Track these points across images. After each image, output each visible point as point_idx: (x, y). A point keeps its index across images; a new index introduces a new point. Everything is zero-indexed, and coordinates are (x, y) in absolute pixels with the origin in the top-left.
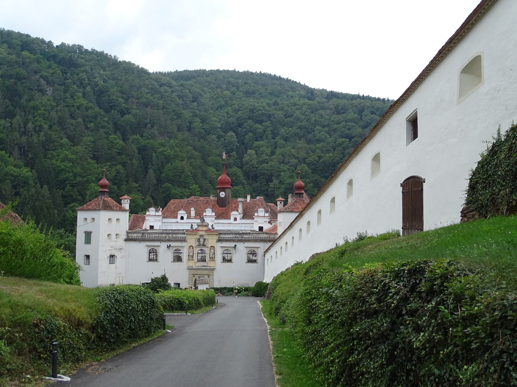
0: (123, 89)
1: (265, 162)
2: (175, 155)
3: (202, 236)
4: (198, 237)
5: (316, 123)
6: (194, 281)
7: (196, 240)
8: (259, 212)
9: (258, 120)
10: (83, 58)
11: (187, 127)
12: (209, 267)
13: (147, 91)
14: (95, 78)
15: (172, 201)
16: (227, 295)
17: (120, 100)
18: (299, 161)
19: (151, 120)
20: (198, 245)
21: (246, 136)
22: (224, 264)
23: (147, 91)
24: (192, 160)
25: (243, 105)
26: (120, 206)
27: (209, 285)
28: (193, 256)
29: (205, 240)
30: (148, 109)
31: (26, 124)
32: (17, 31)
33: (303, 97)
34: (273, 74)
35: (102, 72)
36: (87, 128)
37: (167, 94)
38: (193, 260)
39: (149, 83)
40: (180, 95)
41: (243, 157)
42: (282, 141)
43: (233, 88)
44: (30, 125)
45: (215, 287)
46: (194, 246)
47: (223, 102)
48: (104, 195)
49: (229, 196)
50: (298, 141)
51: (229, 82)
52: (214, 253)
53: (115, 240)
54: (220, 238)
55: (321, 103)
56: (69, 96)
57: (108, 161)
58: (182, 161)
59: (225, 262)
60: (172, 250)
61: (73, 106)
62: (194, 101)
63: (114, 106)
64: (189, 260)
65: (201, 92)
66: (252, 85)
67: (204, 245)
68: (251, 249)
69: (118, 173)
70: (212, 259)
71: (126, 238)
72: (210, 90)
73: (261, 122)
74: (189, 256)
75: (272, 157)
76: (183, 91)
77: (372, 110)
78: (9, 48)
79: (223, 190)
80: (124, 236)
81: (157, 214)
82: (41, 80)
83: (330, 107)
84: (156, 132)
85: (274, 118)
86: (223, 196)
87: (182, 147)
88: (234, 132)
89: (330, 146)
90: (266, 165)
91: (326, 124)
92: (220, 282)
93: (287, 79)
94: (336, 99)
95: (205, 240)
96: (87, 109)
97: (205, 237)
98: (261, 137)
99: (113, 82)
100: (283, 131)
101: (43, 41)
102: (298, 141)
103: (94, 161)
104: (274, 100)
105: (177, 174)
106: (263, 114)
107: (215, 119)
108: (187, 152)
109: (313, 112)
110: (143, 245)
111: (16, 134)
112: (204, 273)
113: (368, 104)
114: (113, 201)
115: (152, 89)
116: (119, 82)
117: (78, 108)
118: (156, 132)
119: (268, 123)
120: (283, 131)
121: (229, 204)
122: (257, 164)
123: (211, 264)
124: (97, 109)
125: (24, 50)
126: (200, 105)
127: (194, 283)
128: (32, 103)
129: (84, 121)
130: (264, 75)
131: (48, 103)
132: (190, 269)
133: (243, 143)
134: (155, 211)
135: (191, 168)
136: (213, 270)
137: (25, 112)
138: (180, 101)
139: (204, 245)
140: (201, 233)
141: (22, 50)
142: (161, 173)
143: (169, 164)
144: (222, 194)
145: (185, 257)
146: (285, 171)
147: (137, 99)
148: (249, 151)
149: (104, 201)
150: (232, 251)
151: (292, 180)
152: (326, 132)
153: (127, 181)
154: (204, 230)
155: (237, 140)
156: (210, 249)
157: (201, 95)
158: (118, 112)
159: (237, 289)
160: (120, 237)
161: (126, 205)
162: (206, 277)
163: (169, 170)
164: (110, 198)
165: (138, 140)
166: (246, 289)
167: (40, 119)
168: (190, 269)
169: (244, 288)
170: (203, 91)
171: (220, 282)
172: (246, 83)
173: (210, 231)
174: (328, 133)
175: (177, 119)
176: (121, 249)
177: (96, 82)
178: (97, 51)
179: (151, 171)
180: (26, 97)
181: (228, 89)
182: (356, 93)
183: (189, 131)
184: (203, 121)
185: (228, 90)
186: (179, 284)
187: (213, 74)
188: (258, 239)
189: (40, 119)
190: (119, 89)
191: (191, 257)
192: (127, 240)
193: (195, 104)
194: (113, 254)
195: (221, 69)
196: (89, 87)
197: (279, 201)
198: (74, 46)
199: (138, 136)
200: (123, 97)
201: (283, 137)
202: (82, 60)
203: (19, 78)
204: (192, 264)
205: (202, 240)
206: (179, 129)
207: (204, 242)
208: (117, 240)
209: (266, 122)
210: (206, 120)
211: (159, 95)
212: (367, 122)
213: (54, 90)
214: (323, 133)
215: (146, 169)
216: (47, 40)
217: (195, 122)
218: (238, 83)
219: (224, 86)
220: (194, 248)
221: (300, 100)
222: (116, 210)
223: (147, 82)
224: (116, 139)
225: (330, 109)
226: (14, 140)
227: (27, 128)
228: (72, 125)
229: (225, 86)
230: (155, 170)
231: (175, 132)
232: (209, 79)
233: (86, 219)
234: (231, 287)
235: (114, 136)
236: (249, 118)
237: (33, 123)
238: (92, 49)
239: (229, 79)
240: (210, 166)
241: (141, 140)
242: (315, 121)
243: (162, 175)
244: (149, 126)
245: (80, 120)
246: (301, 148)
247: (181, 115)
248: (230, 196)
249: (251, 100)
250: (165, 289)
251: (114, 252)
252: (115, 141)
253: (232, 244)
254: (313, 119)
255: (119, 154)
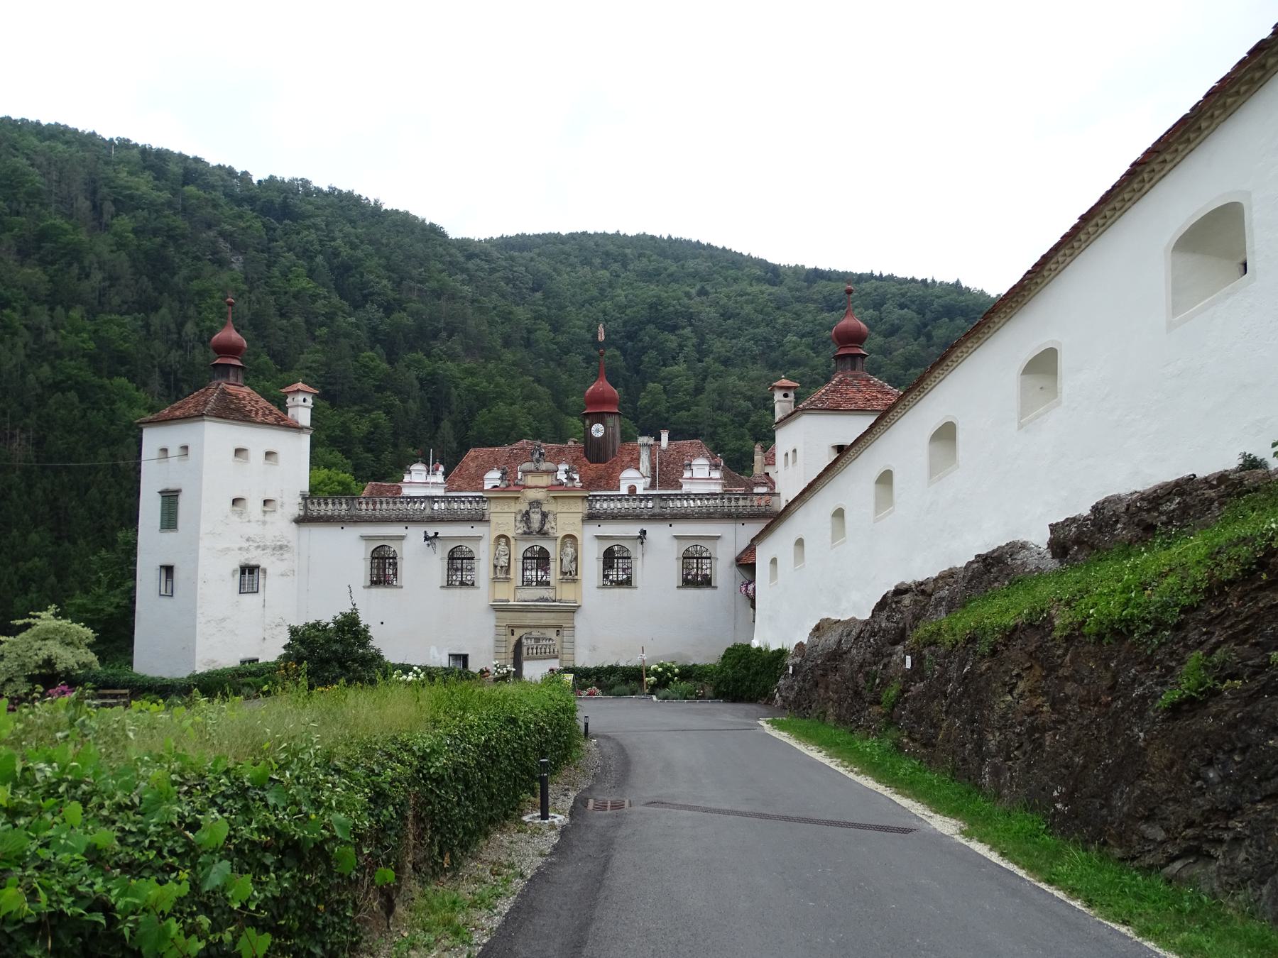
0: (391, 263)
1: (684, 409)
2: (497, 392)
3: (535, 503)
4: (525, 507)
5: (786, 330)
6: (511, 648)
7: (519, 517)
8: (693, 467)
9: (668, 325)
10: (310, 203)
11: (522, 338)
12: (560, 601)
13: (440, 266)
14: (334, 239)
15: (472, 452)
16: (619, 695)
17: (385, 282)
18: (755, 406)
19: (447, 324)
20: (525, 533)
21: (643, 358)
22: (607, 591)
23: (440, 266)
24: (532, 402)
25: (636, 296)
26: (280, 413)
27: (562, 660)
28: (507, 569)
29: (545, 516)
30: (442, 302)
31: (180, 326)
32: (176, 151)
33: (759, 280)
34: (694, 240)
35: (348, 229)
36: (314, 338)
37: (481, 274)
38: (508, 580)
39: (444, 253)
40: (508, 278)
41: (638, 399)
42: (717, 364)
43: (616, 264)
44: (190, 328)
45: (579, 664)
46: (510, 535)
47: (595, 292)
48: (228, 376)
49: (614, 435)
50: (750, 366)
51: (607, 254)
52: (576, 559)
53: (260, 517)
54: (594, 511)
55: (797, 290)
56: (277, 274)
57: (355, 404)
58: (512, 404)
59: (611, 587)
60: (442, 551)
61: (286, 293)
62: (534, 290)
63: (372, 294)
64: (495, 579)
65: (550, 271)
66: (654, 257)
67: (542, 533)
68: (695, 542)
69: (376, 426)
70: (570, 576)
71: (302, 513)
72: (569, 269)
73: (674, 329)
74: (495, 566)
75: (698, 398)
76: (515, 269)
77: (902, 300)
78: (156, 179)
79: (600, 418)
80: (294, 507)
81: (432, 479)
82: (221, 240)
83: (815, 297)
84: (458, 348)
85: (700, 320)
86: (600, 435)
87: (513, 377)
88: (618, 348)
89: (818, 374)
90: (686, 413)
91: (808, 329)
92: (594, 649)
93: (724, 248)
94: (824, 282)
95: (545, 516)
96: (315, 298)
97: (545, 508)
98: (674, 358)
99: (371, 249)
100: (718, 346)
101: (230, 172)
102: (750, 366)
103: (327, 404)
104: (698, 287)
105: (501, 430)
106: (676, 313)
107: (578, 323)
108: (522, 386)
109: (778, 308)
110: (351, 535)
111: (158, 346)
112: (543, 623)
113: (893, 290)
114: (256, 396)
115: (451, 263)
116: (383, 249)
117: (296, 297)
118: (458, 348)
119: (687, 331)
120: (718, 346)
121: (614, 455)
122: (668, 412)
123: (566, 593)
124: (335, 299)
125: (188, 184)
126: (549, 298)
127: (512, 655)
128: (196, 285)
129: (307, 321)
130: (679, 242)
131: (233, 284)
132: (499, 608)
133: (638, 372)
134: (425, 473)
135: (530, 418)
136: (573, 610)
137: (181, 302)
138: (509, 289)
139: (542, 533)
140: (532, 495)
141: (185, 183)
142: (468, 428)
143: (484, 410)
144: (598, 430)
145: (483, 569)
146: (725, 425)
147: (420, 282)
148: (650, 385)
149: (223, 392)
150: (635, 549)
151: (741, 442)
152: (808, 346)
153: (395, 446)
154: (543, 484)
155: (624, 364)
156: (563, 545)
157: (551, 278)
158: (380, 306)
159: (655, 673)
160: (279, 510)
161: (302, 411)
162: (551, 633)
163: (484, 423)
164: (247, 389)
165: (419, 361)
166: (688, 673)
167: (211, 316)
168: (499, 608)
169: (679, 668)
170: (555, 270)
171: (594, 649)
172: (640, 255)
173: (562, 488)
174: (812, 349)
175: (502, 323)
176: (281, 547)
177: (336, 249)
178: (340, 191)
179: (446, 425)
180: (184, 272)
181: (604, 266)
182: (867, 271)
183: (526, 347)
184: (556, 328)
185: (606, 269)
186: (465, 658)
187: (574, 239)
188: (716, 512)
189: (211, 316)
190: (383, 262)
191: (501, 572)
192: (304, 520)
193: (539, 295)
194: (253, 563)
195: (591, 232)
196: (321, 257)
197: (781, 388)
198: (292, 181)
199: (420, 355)
200: (389, 279)
201: (719, 357)
202: (309, 207)
203: (172, 236)
204: (506, 593)
205: (536, 518)
206: (507, 343)
207: (543, 522)
208: (268, 518)
209: (684, 328)
210: (562, 326)
211: (465, 276)
212: (892, 325)
213: (245, 259)
214: (803, 348)
215: (437, 421)
216: (239, 169)
217: (539, 329)
218: (626, 255)
219: (597, 261)
220: (512, 542)
221: (751, 285)
222: (264, 424)
223: (440, 249)
224: (375, 358)
225: (815, 301)
226: (152, 357)
227: (183, 334)
228: (281, 330)
229: (599, 261)
230: (454, 424)
231: (499, 348)
232: (567, 248)
233: (165, 450)
234: (632, 664)
235: (371, 353)
236: (649, 322)
237: (197, 325)
238: (330, 188)
239: (608, 248)
240: (572, 416)
241: (426, 361)
242: (785, 324)
243: (470, 433)
244: (444, 334)
245: (298, 320)
246: (758, 379)
247: (511, 316)
248: (618, 435)
249: (652, 287)
250: (356, 679)
251: (253, 558)
252: (372, 364)
253: (633, 529)
254: (781, 320)
255: (379, 389)
